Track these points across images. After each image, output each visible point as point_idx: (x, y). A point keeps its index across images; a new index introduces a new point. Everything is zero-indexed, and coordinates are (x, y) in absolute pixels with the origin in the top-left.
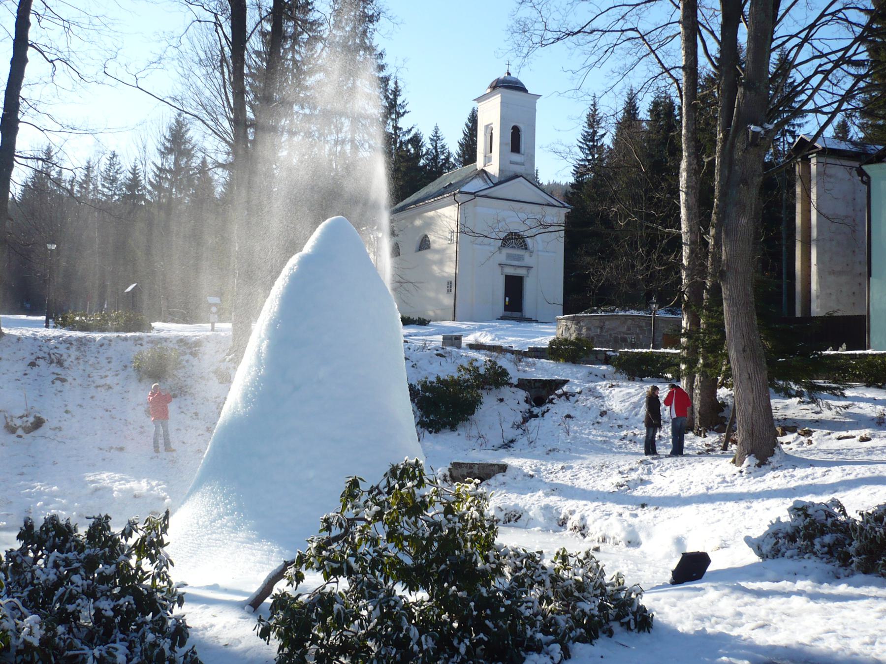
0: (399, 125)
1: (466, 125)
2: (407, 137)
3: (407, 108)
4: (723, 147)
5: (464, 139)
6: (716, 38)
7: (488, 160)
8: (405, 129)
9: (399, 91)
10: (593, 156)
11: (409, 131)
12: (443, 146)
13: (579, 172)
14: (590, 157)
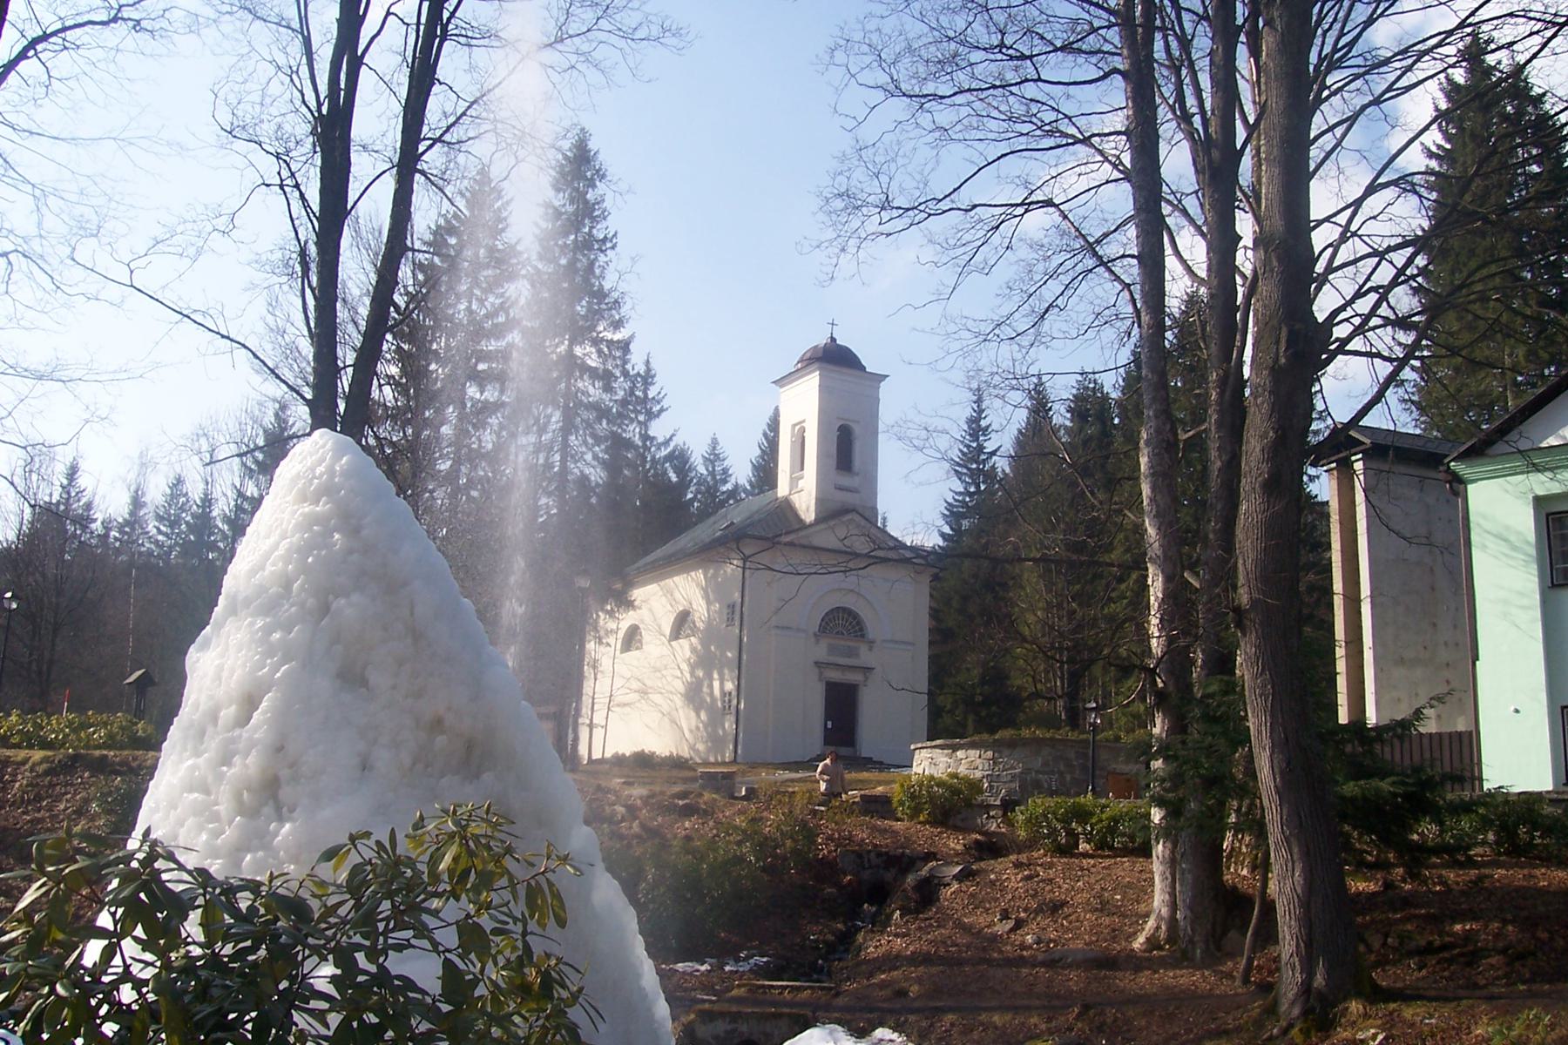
0: (651, 433)
1: (765, 435)
2: (664, 452)
3: (665, 404)
4: (1221, 395)
5: (762, 457)
6: (1192, 221)
7: (794, 481)
8: (661, 440)
9: (653, 377)
10: (978, 486)
11: (667, 443)
12: (725, 471)
13: (954, 515)
14: (972, 489)
